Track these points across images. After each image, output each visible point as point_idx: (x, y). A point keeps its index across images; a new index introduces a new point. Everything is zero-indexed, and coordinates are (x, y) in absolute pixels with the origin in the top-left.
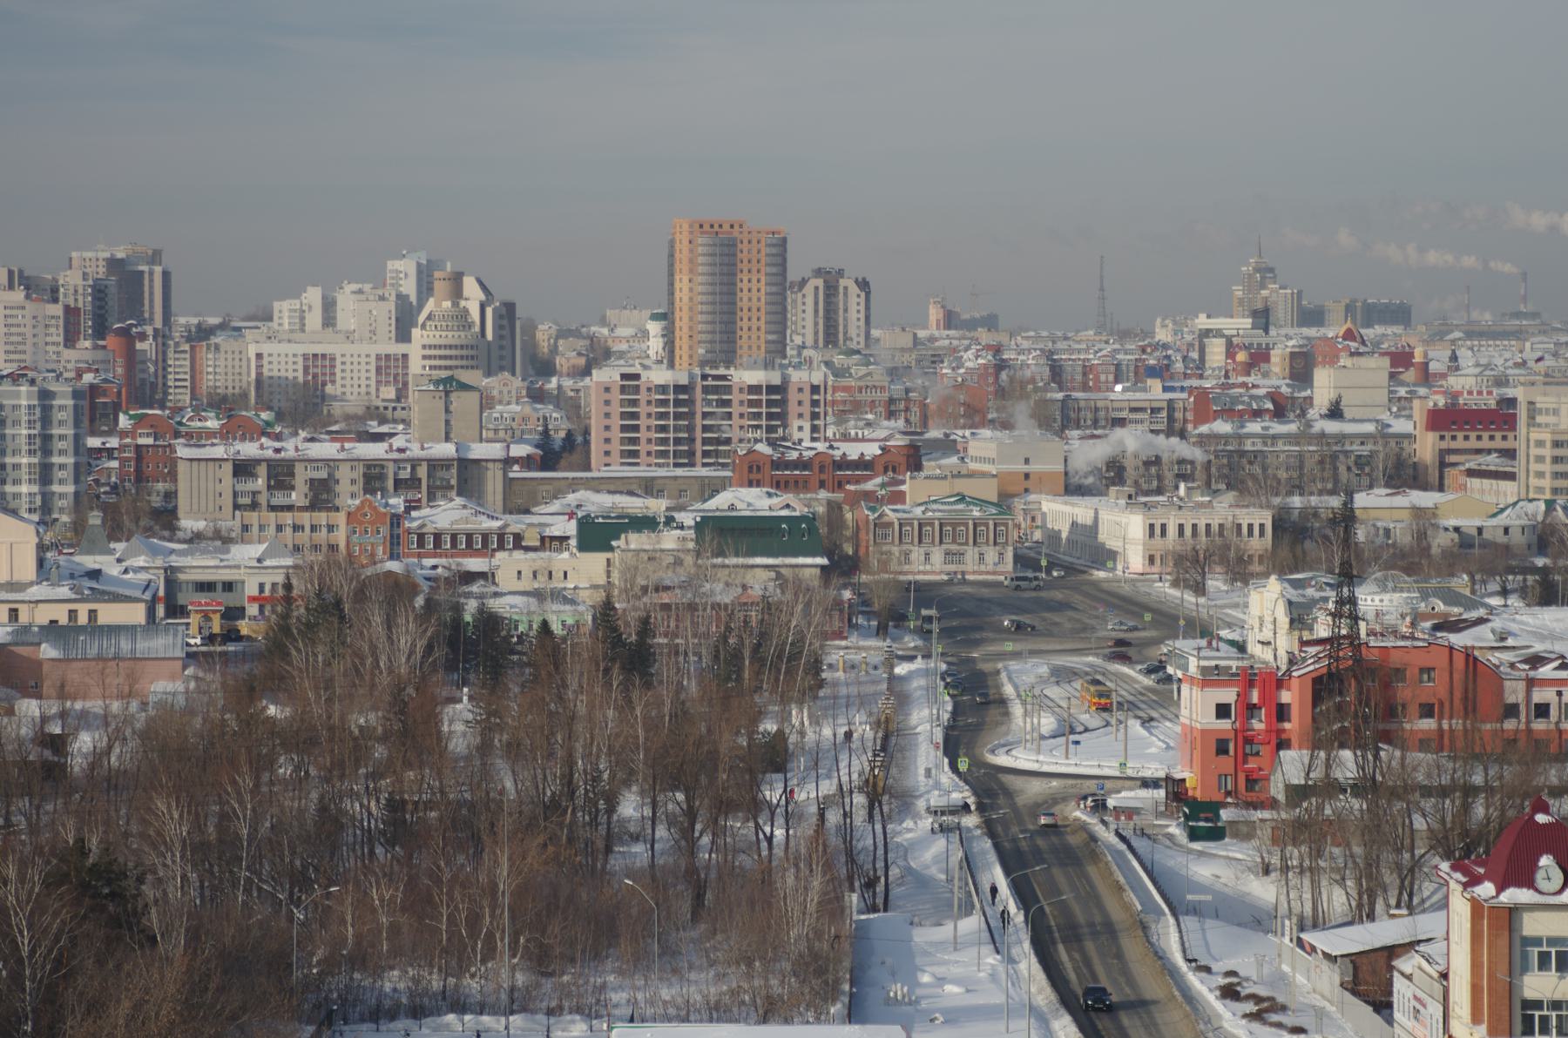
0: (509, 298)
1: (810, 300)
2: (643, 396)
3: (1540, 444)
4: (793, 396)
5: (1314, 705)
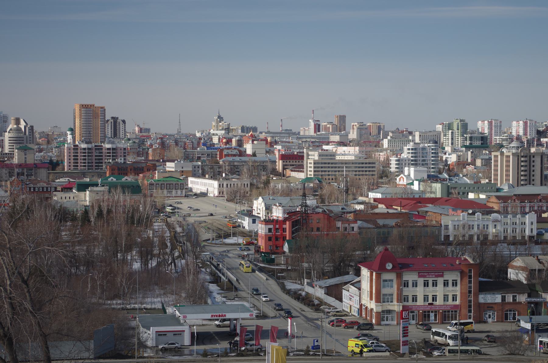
0: (32, 125)
1: (110, 125)
2: (79, 151)
3: (310, 163)
4: (119, 151)
5: (292, 228)
